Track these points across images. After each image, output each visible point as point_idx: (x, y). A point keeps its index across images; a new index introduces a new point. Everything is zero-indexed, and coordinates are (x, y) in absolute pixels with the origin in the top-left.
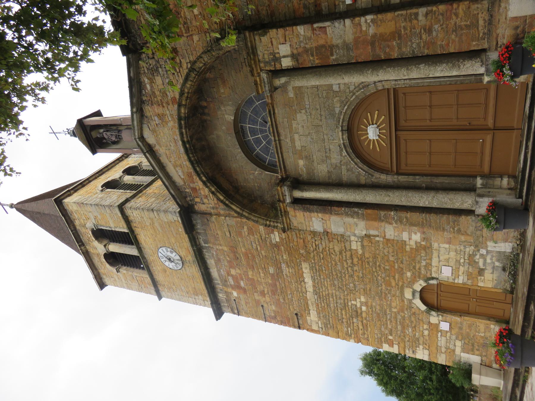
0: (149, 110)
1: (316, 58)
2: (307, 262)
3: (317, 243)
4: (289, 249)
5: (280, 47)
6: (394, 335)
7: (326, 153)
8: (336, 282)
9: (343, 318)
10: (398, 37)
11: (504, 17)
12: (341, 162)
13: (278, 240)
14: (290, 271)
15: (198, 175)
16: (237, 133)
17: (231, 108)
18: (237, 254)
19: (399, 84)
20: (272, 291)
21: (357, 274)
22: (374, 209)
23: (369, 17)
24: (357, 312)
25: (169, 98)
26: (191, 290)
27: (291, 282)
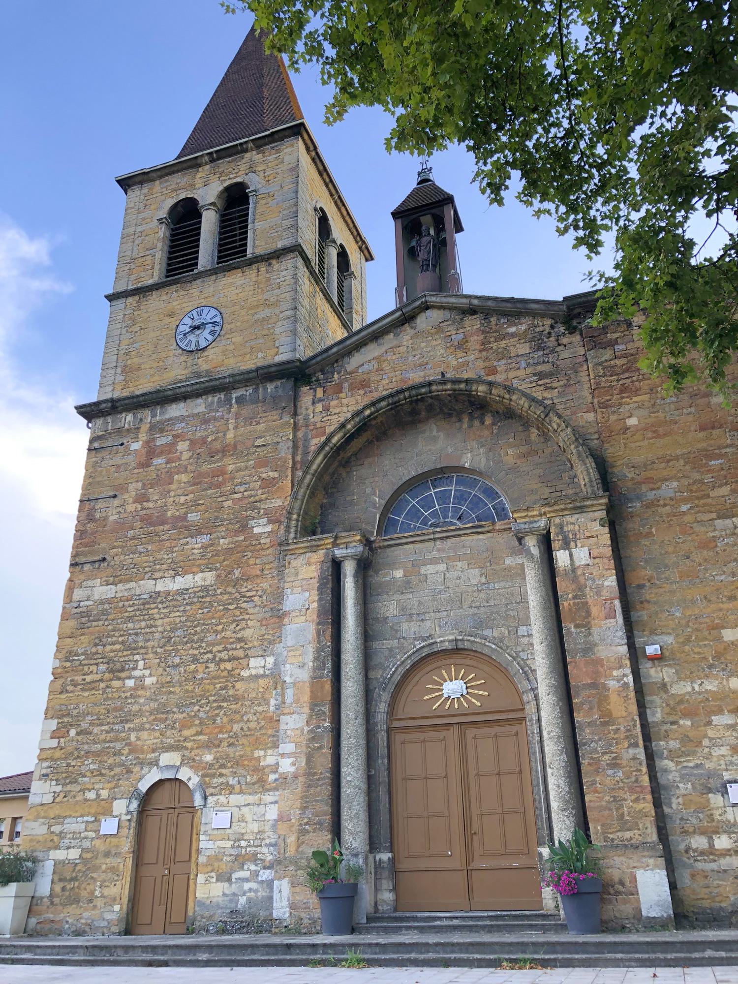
0: (473, 324)
1: (571, 602)
2: (216, 580)
3: (256, 599)
4: (239, 549)
5: (586, 549)
6: (79, 738)
7: (418, 614)
8: (179, 633)
9: (104, 646)
10: (605, 722)
11: (635, 865)
12: (404, 638)
13: (256, 530)
14: (196, 551)
15: (373, 404)
16: (442, 470)
17: (483, 465)
18: (220, 455)
19: (532, 725)
20: (150, 516)
21: (201, 670)
22: (332, 694)
23: (630, 679)
24: (122, 670)
25: (495, 364)
26: (134, 360)
27: (173, 552)
